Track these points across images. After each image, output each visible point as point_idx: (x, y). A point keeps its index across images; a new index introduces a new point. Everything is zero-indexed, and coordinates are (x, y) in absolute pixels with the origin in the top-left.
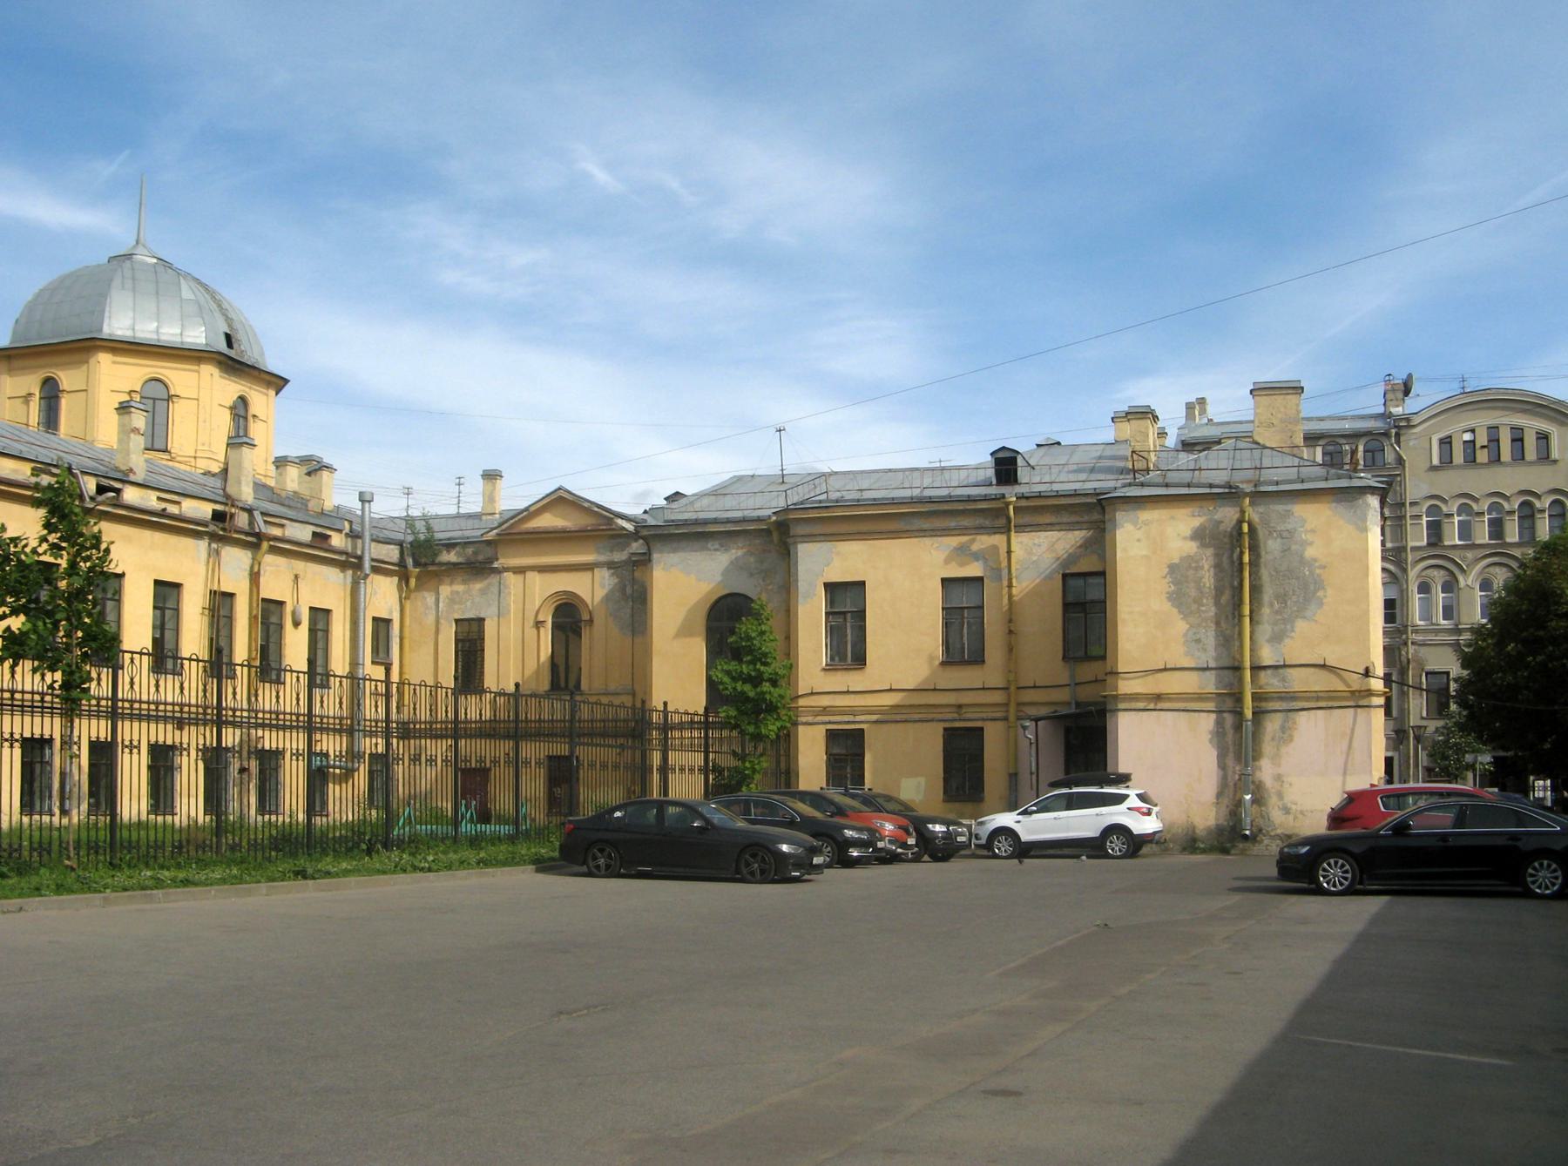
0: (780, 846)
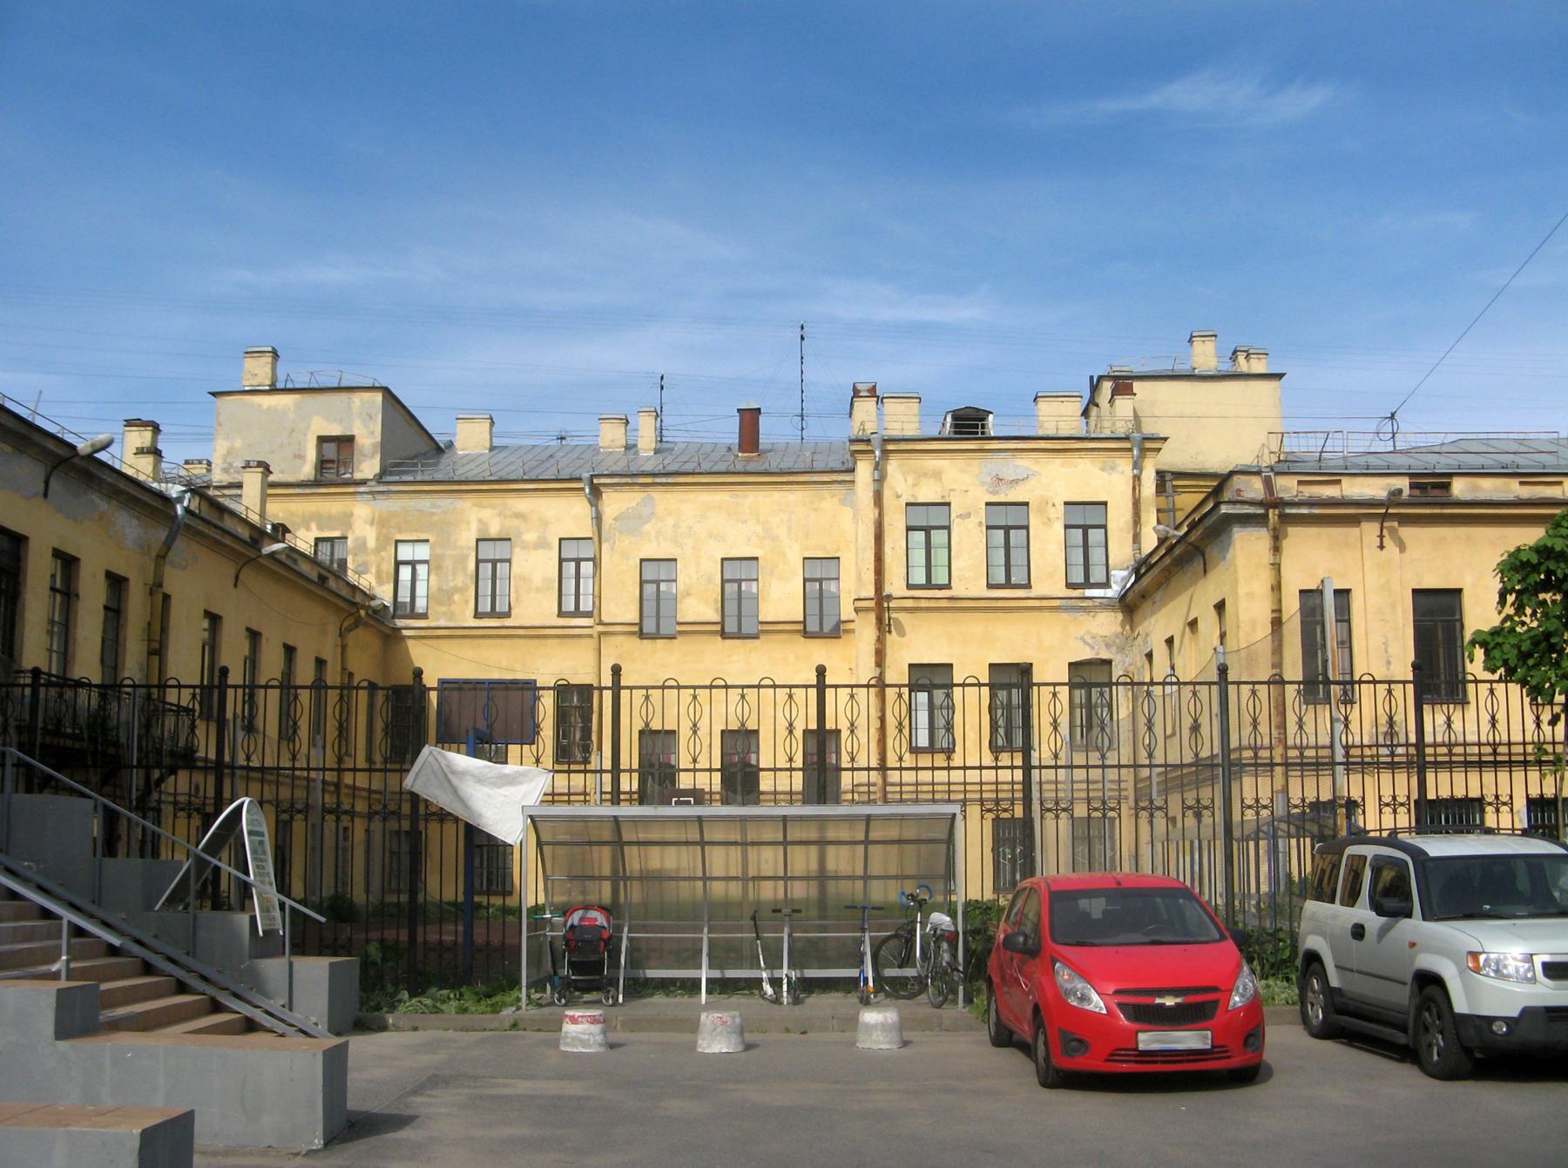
0: (1231, 1003)
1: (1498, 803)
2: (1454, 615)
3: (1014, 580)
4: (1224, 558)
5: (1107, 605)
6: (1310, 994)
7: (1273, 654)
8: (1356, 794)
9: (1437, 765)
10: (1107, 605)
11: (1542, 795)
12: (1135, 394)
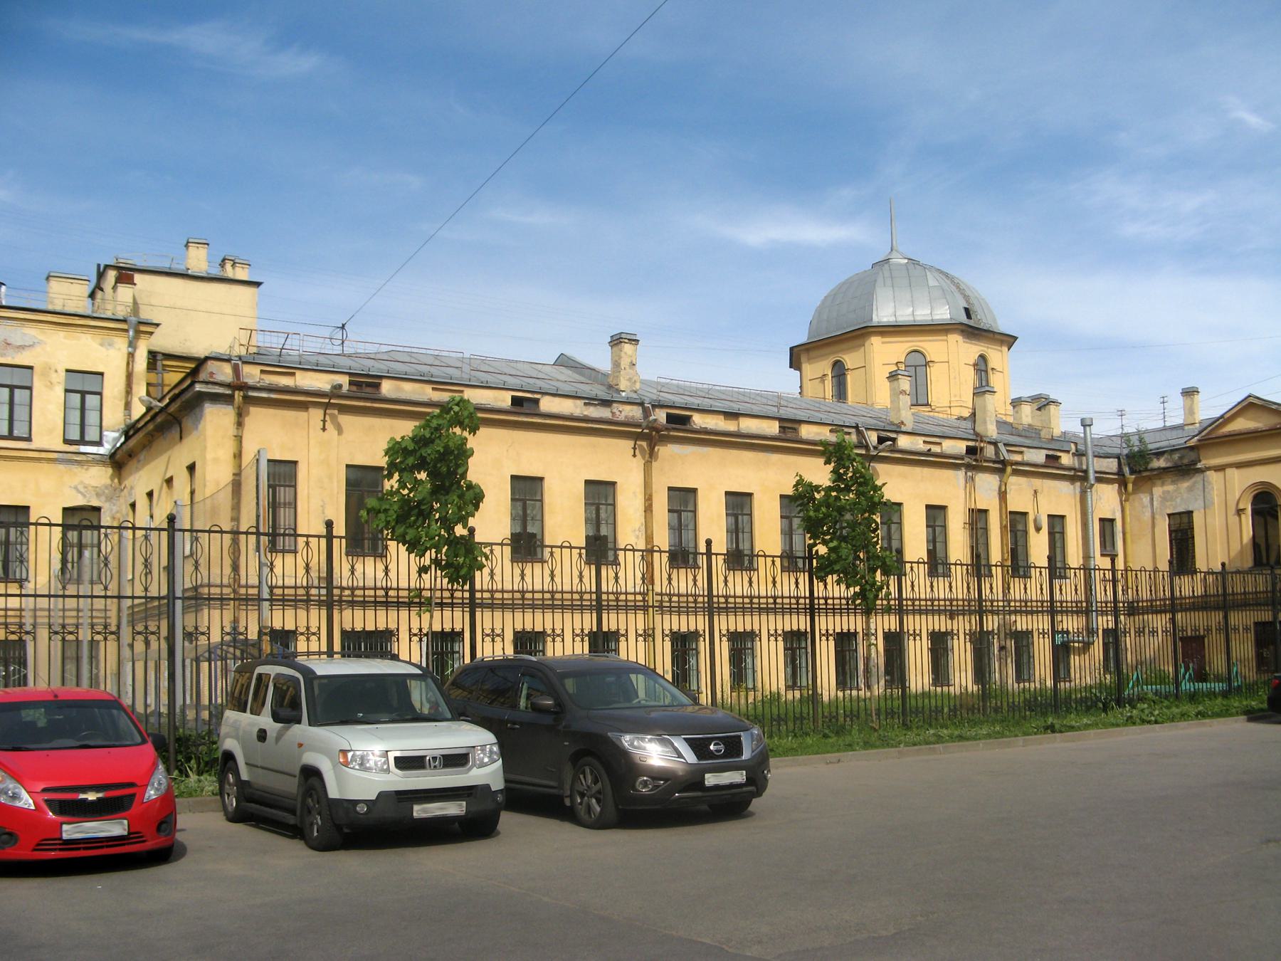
1: (308, 634)
2: (535, 495)
3: (16, 433)
4: (197, 428)
5: (99, 460)
6: (227, 787)
7: (232, 509)
8: (392, 626)
9: (483, 606)
10: (99, 460)
11: (353, 629)
12: (135, 284)
